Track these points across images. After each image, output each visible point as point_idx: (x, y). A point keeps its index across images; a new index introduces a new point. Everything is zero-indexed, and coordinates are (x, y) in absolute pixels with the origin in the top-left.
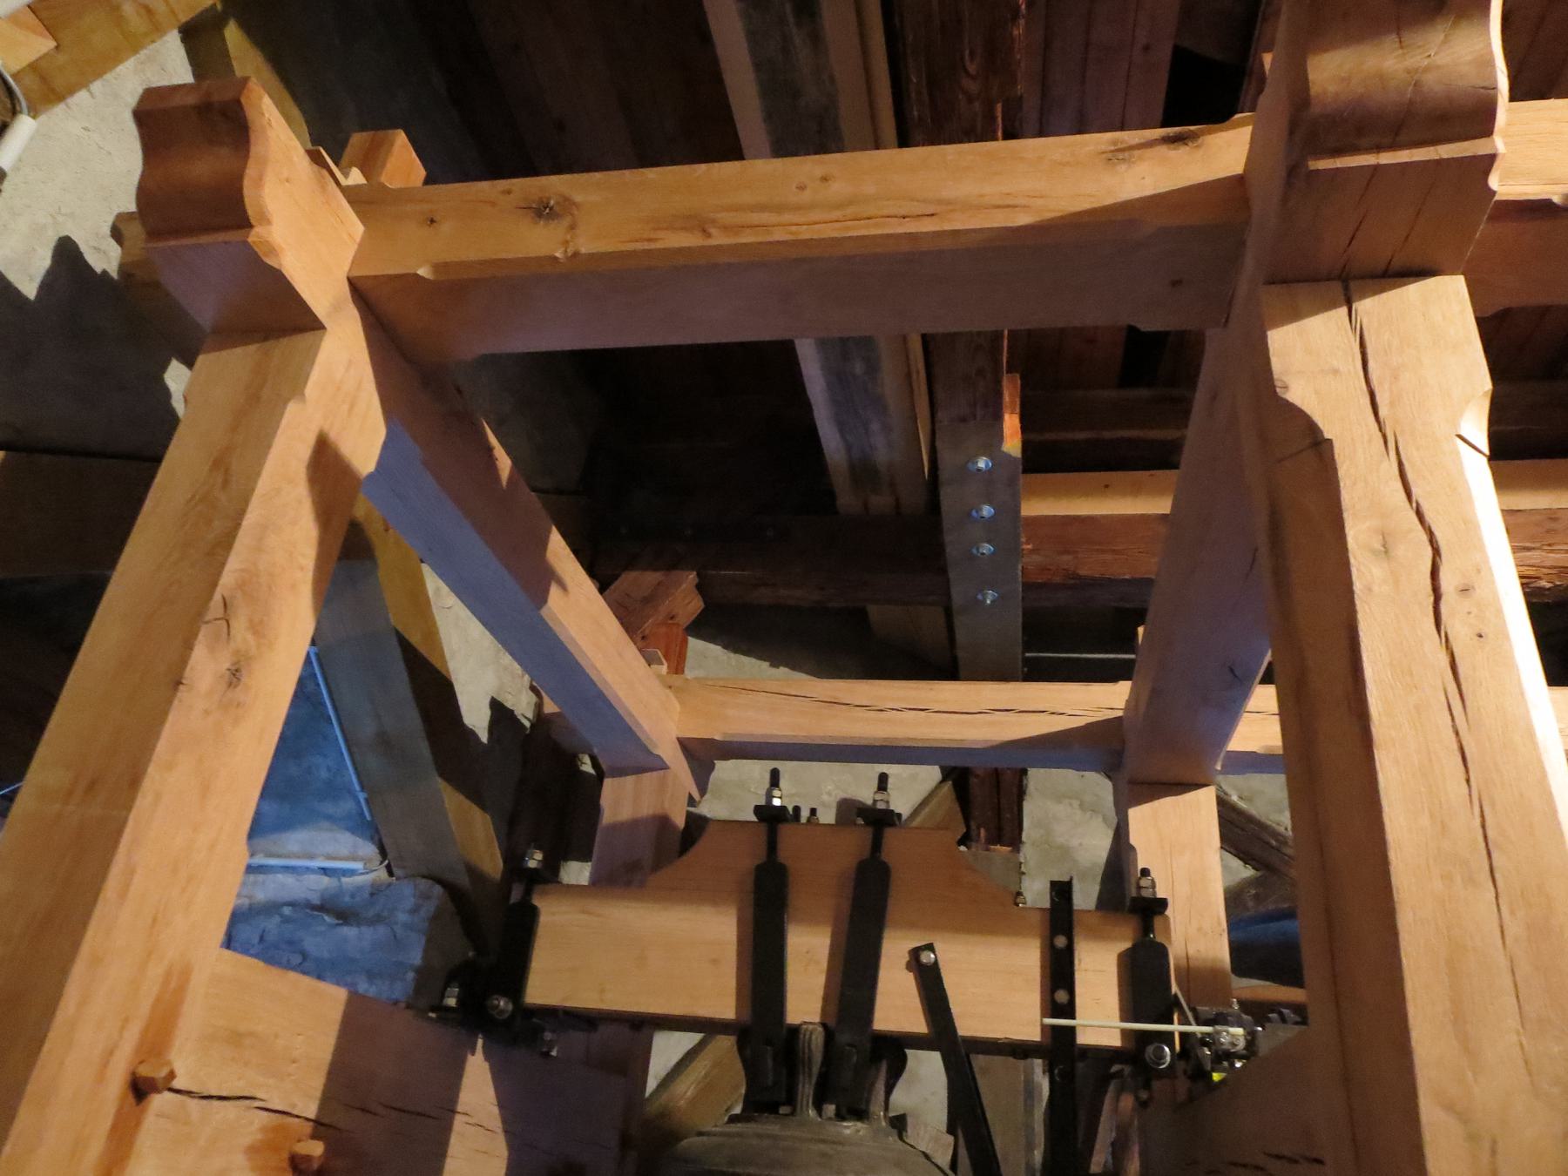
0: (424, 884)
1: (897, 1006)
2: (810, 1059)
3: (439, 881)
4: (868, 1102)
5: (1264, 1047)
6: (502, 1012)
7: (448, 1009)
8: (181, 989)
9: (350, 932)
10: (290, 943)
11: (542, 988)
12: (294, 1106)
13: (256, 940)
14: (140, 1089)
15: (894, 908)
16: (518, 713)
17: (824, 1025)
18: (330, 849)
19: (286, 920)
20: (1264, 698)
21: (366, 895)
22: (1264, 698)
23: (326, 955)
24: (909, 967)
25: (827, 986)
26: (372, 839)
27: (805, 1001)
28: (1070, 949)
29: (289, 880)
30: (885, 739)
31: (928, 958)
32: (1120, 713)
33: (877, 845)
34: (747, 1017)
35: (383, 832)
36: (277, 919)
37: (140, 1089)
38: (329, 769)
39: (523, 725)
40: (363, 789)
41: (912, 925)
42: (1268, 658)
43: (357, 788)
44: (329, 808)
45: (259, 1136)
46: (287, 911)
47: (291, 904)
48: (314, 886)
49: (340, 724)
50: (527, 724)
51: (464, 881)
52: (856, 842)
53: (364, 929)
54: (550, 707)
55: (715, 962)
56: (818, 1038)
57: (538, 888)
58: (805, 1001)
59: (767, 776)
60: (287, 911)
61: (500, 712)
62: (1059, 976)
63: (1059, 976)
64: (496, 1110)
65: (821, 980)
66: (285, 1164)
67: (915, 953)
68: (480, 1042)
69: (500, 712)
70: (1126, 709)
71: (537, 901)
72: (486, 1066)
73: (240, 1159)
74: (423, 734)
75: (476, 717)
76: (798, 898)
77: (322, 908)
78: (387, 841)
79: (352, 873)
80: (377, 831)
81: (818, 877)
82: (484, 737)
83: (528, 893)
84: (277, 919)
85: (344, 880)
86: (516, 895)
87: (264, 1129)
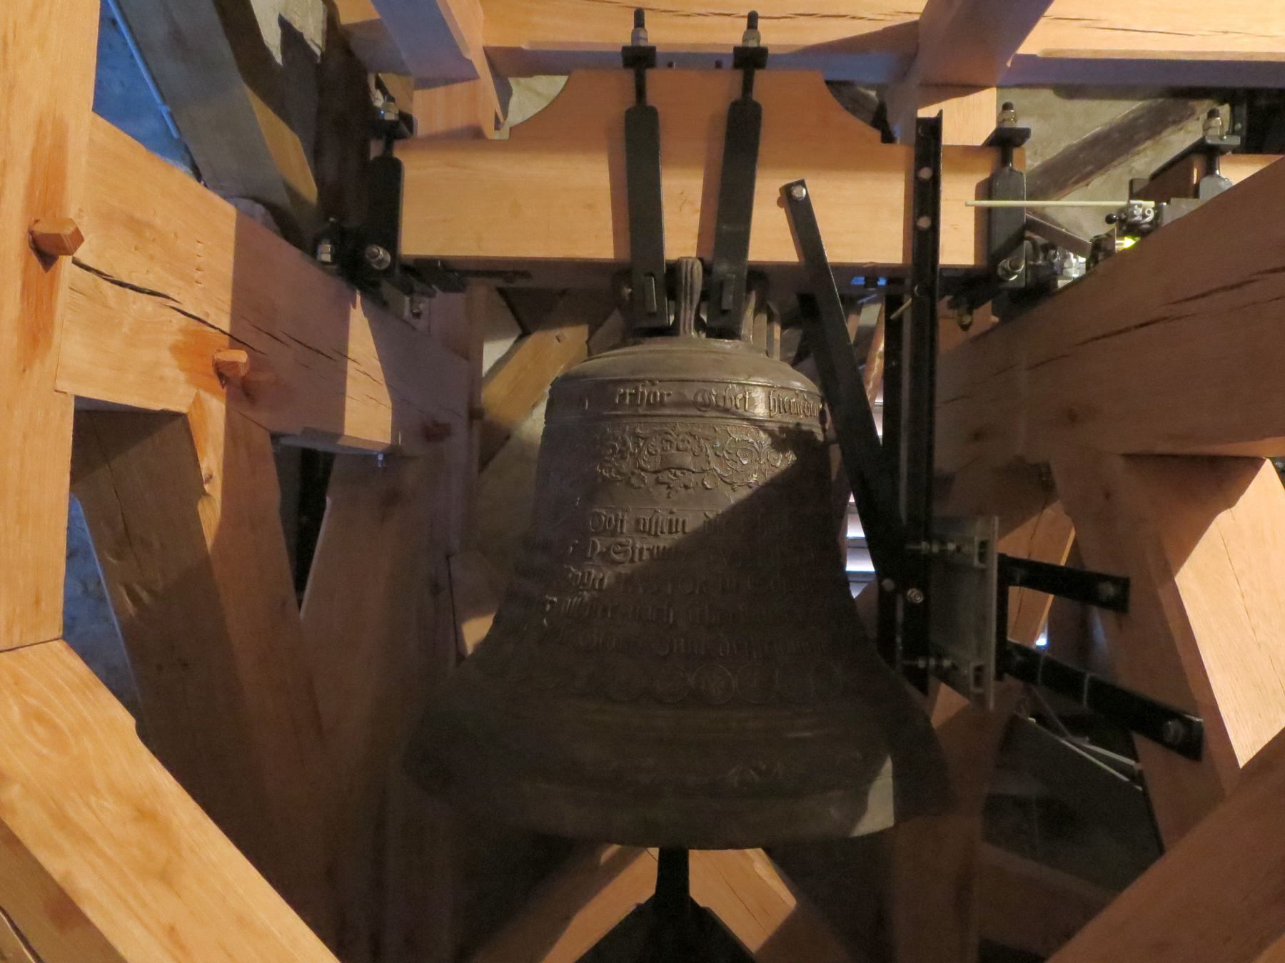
0: (246, 203)
1: (770, 241)
2: (692, 287)
3: (256, 200)
4: (739, 323)
5: (1167, 219)
6: (381, 262)
7: (325, 263)
8: (60, 145)
11: (423, 233)
12: (207, 315)
14: (46, 250)
15: (766, 148)
16: (307, 37)
17: (701, 259)
24: (780, 203)
25: (702, 226)
26: (183, 159)
27: (681, 237)
28: (935, 182)
30: (694, 45)
31: (800, 193)
32: (917, 18)
33: (748, 86)
34: (626, 256)
35: (193, 152)
37: (46, 250)
38: (122, 84)
39: (313, 53)
40: (165, 101)
41: (780, 165)
42: (302, 614)
43: (158, 100)
45: (180, 337)
49: (130, 28)
50: (318, 52)
51: (283, 199)
52: (725, 87)
55: (590, 206)
56: (698, 268)
57: (398, 144)
58: (681, 237)
59: (632, 18)
61: (290, 34)
62: (925, 200)
63: (925, 200)
64: (378, 364)
65: (695, 219)
66: (211, 371)
67: (787, 191)
68: (358, 298)
69: (290, 34)
70: (923, 15)
71: (397, 154)
72: (366, 321)
73: (166, 356)
74: (220, 29)
75: (272, 37)
76: (669, 142)
78: (200, 161)
80: (187, 150)
81: (691, 112)
83: (389, 147)
86: (375, 149)
87: (183, 331)
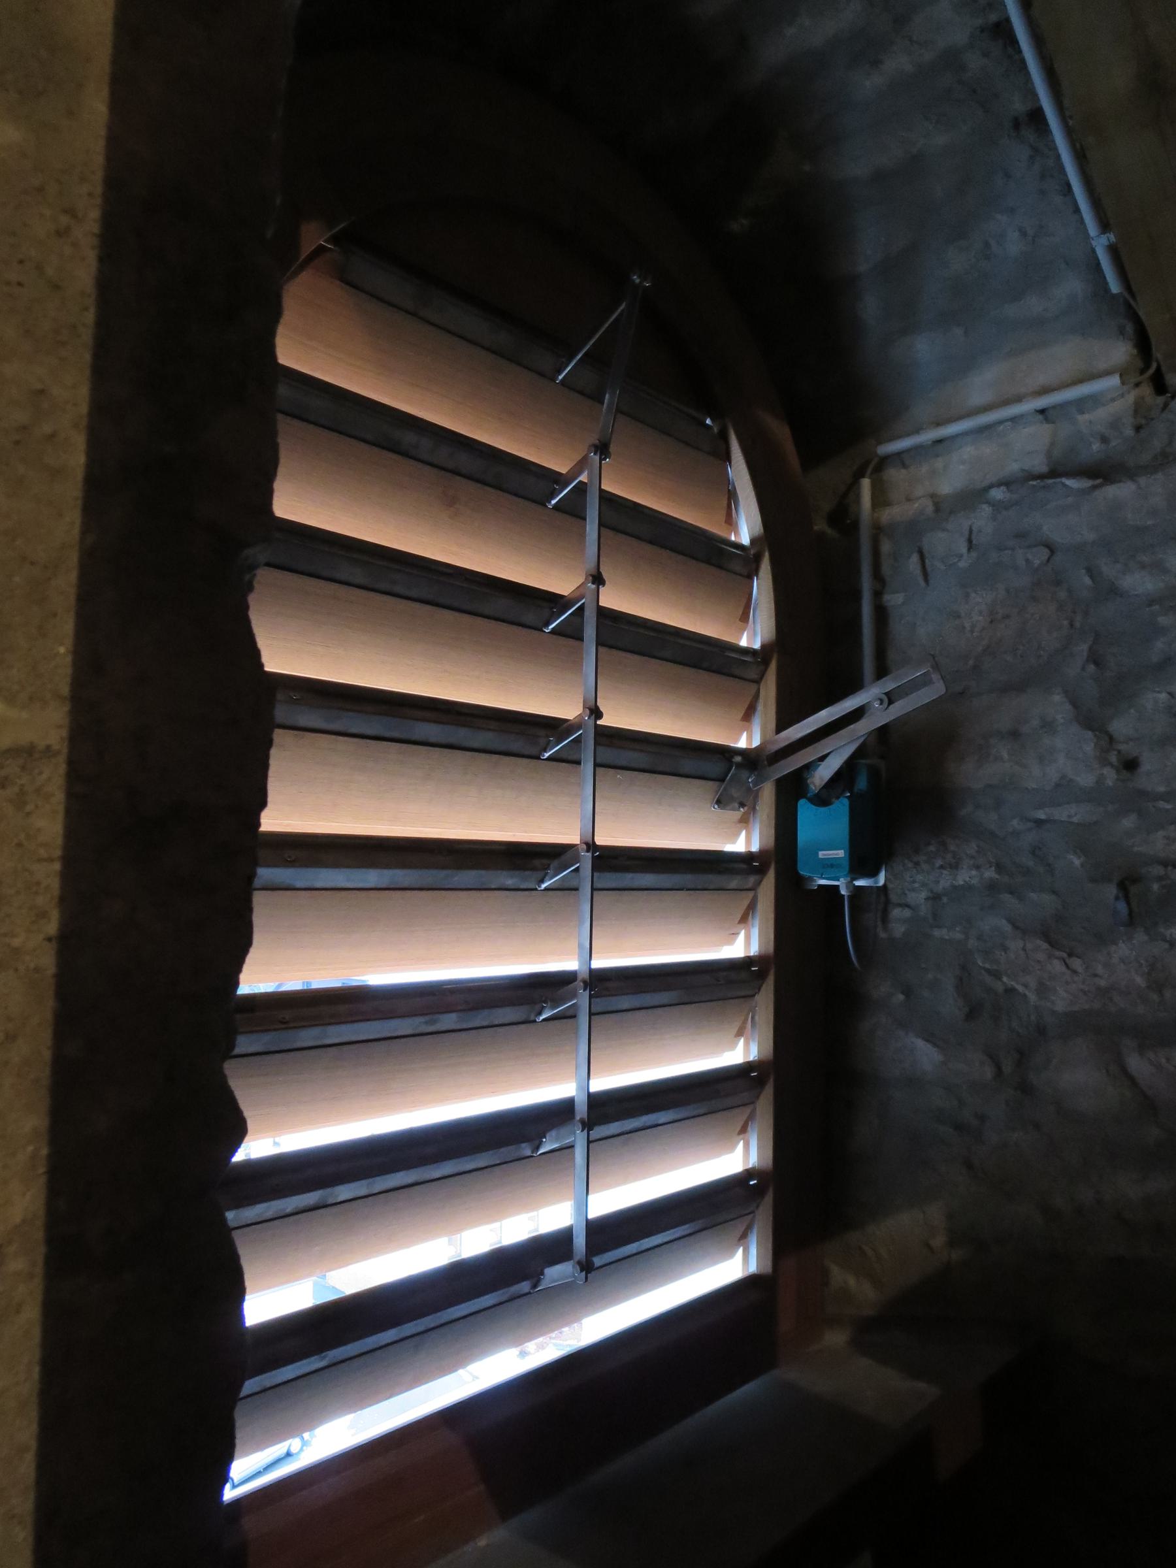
9: (1121, 491)
10: (1021, 535)
13: (964, 550)
18: (1042, 379)
19: (997, 506)
20: (586, 473)
21: (1129, 432)
22: (586, 473)
23: (1090, 536)
29: (987, 449)
36: (986, 510)
40: (1105, 227)
44: (1033, 305)
46: (998, 494)
47: (1006, 483)
48: (1029, 447)
53: (1143, 480)
54: (945, 543)
60: (998, 494)
77: (1054, 473)
79: (1093, 401)
82: (239, 1157)
84: (986, 510)
85: (1082, 419)
